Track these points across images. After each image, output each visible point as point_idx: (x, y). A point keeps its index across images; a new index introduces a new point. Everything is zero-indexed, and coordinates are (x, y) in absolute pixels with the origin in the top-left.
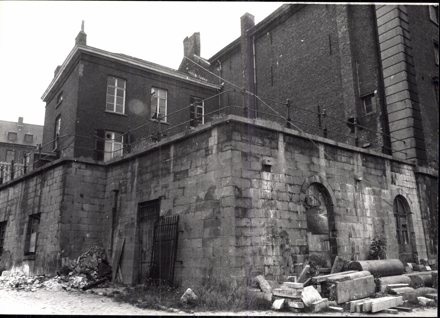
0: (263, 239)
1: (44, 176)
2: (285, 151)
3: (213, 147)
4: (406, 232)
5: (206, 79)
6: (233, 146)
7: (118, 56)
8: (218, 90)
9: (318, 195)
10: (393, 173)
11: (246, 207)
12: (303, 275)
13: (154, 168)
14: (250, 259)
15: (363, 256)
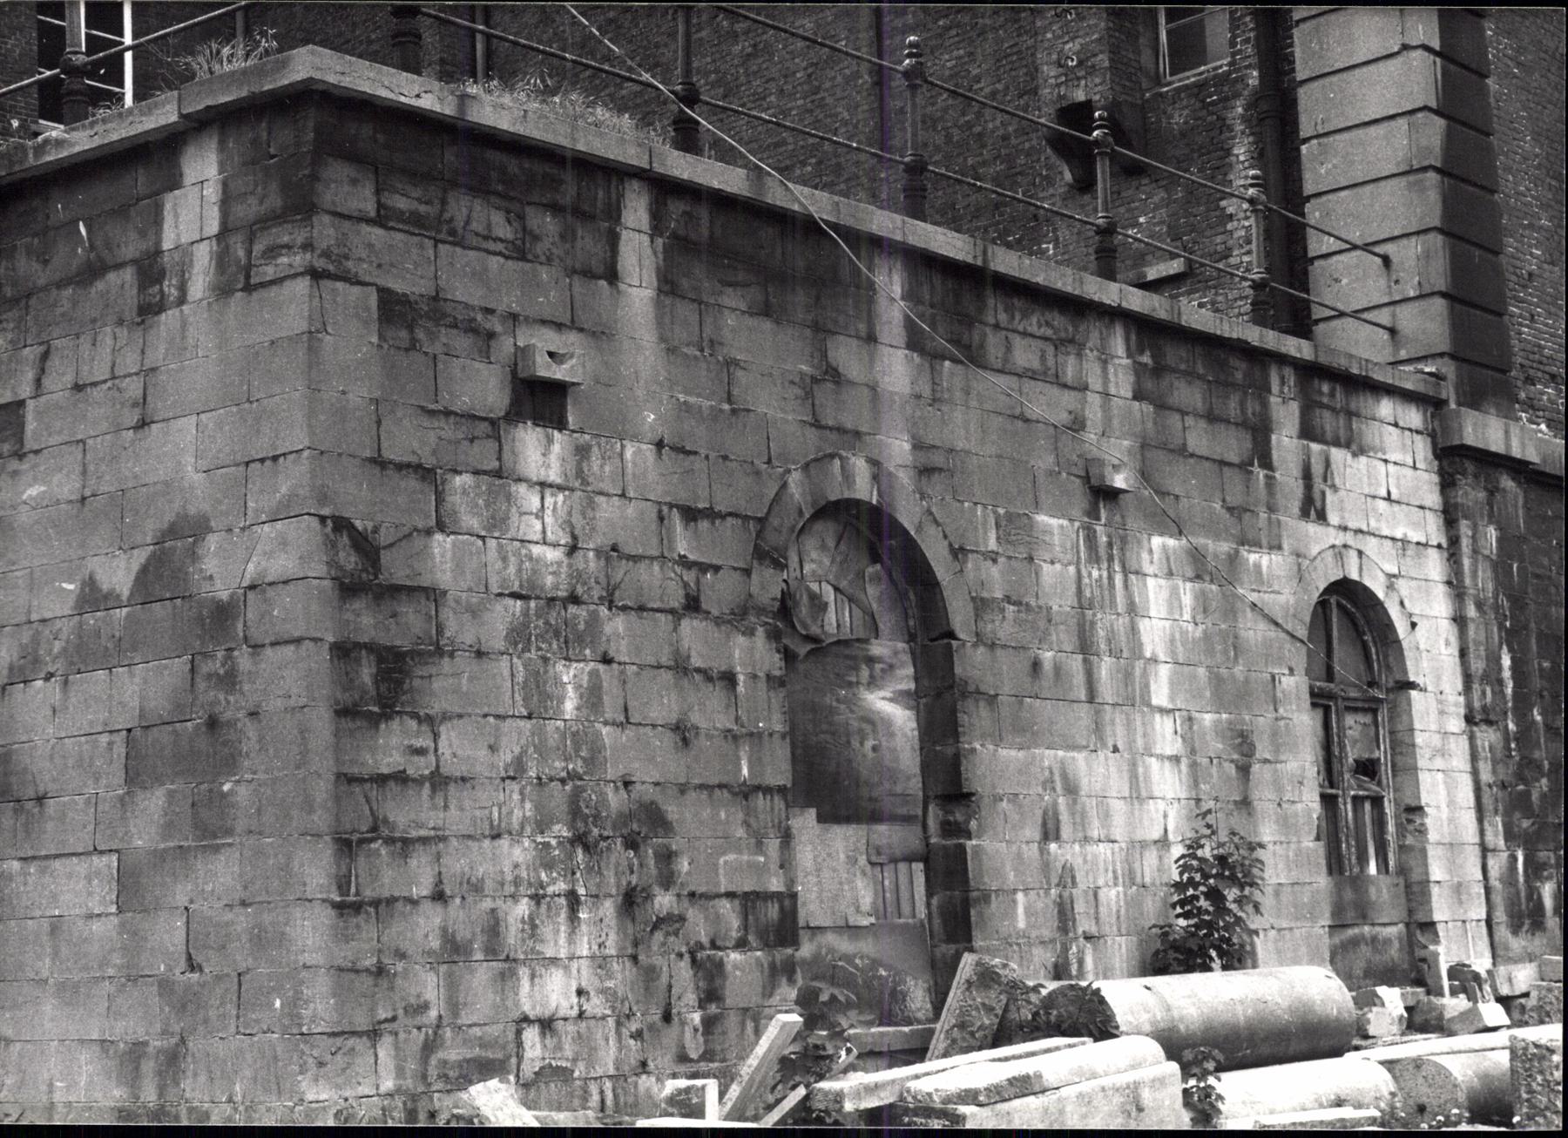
0: (517, 854)
2: (660, 291)
4: (1377, 801)
6: (326, 254)
9: (860, 575)
10: (1315, 447)
11: (404, 644)
12: (758, 1069)
14: (429, 986)
15: (1121, 948)
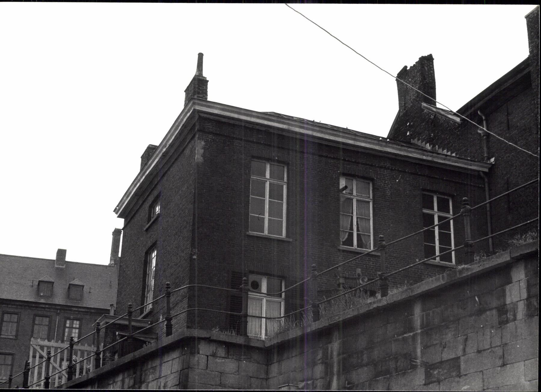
1: (138, 373)
3: (517, 305)
5: (452, 153)
7: (270, 117)
8: (482, 174)
13: (376, 354)
